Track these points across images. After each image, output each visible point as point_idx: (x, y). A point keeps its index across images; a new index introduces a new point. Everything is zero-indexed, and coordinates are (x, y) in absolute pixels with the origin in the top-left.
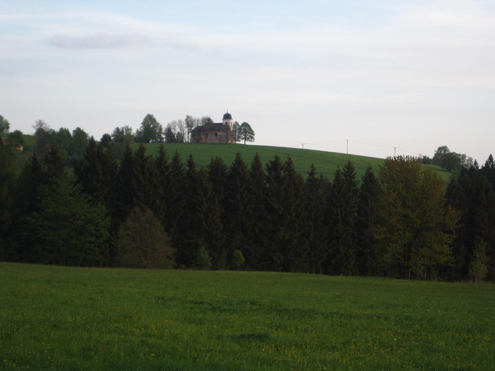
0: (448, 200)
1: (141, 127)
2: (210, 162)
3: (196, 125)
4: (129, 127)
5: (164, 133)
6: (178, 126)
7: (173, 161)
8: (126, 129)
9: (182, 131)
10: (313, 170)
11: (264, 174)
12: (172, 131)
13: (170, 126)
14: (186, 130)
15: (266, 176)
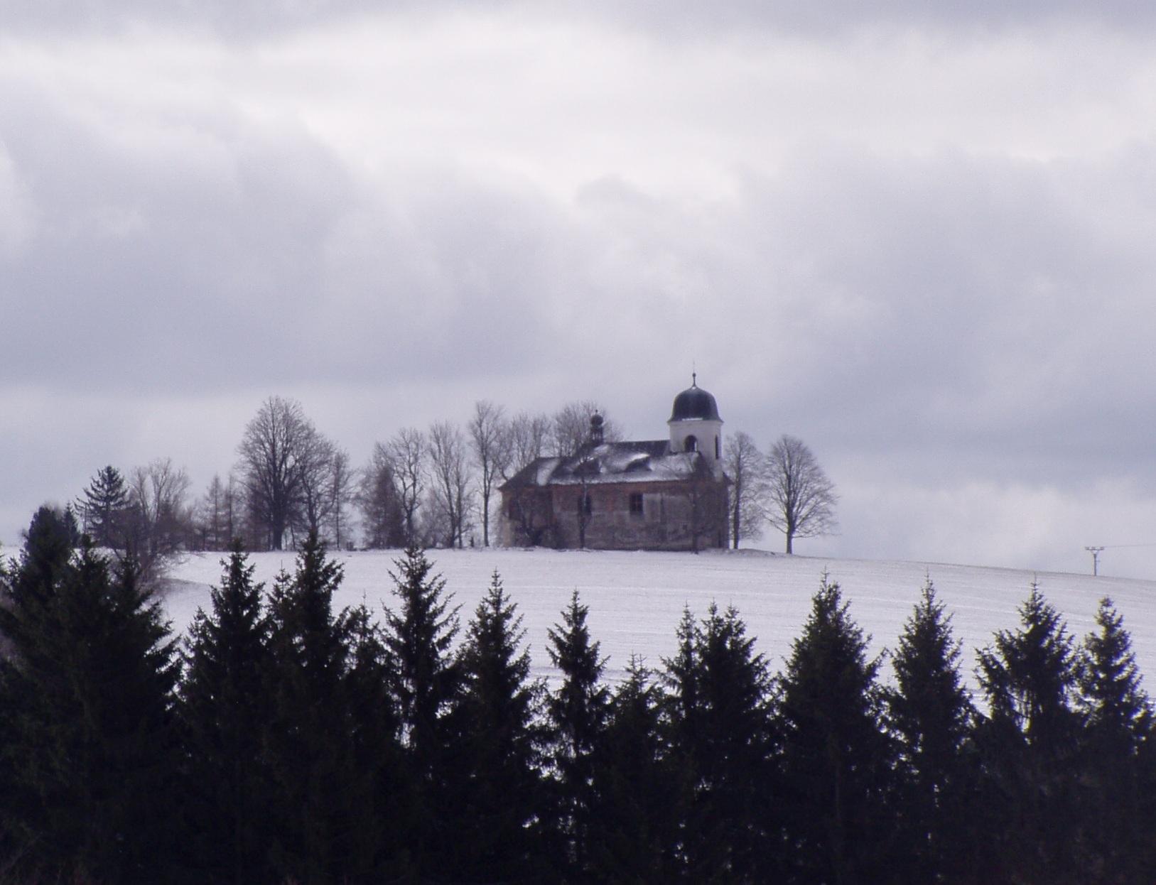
0: (123, 553)
1: (236, 467)
2: (674, 651)
3: (527, 453)
4: (174, 470)
5: (358, 497)
6: (430, 458)
7: (473, 643)
8: (155, 478)
9: (454, 489)
10: (688, 617)
11: (972, 708)
12: (400, 486)
13: (393, 460)
14: (475, 480)
15: (980, 718)
